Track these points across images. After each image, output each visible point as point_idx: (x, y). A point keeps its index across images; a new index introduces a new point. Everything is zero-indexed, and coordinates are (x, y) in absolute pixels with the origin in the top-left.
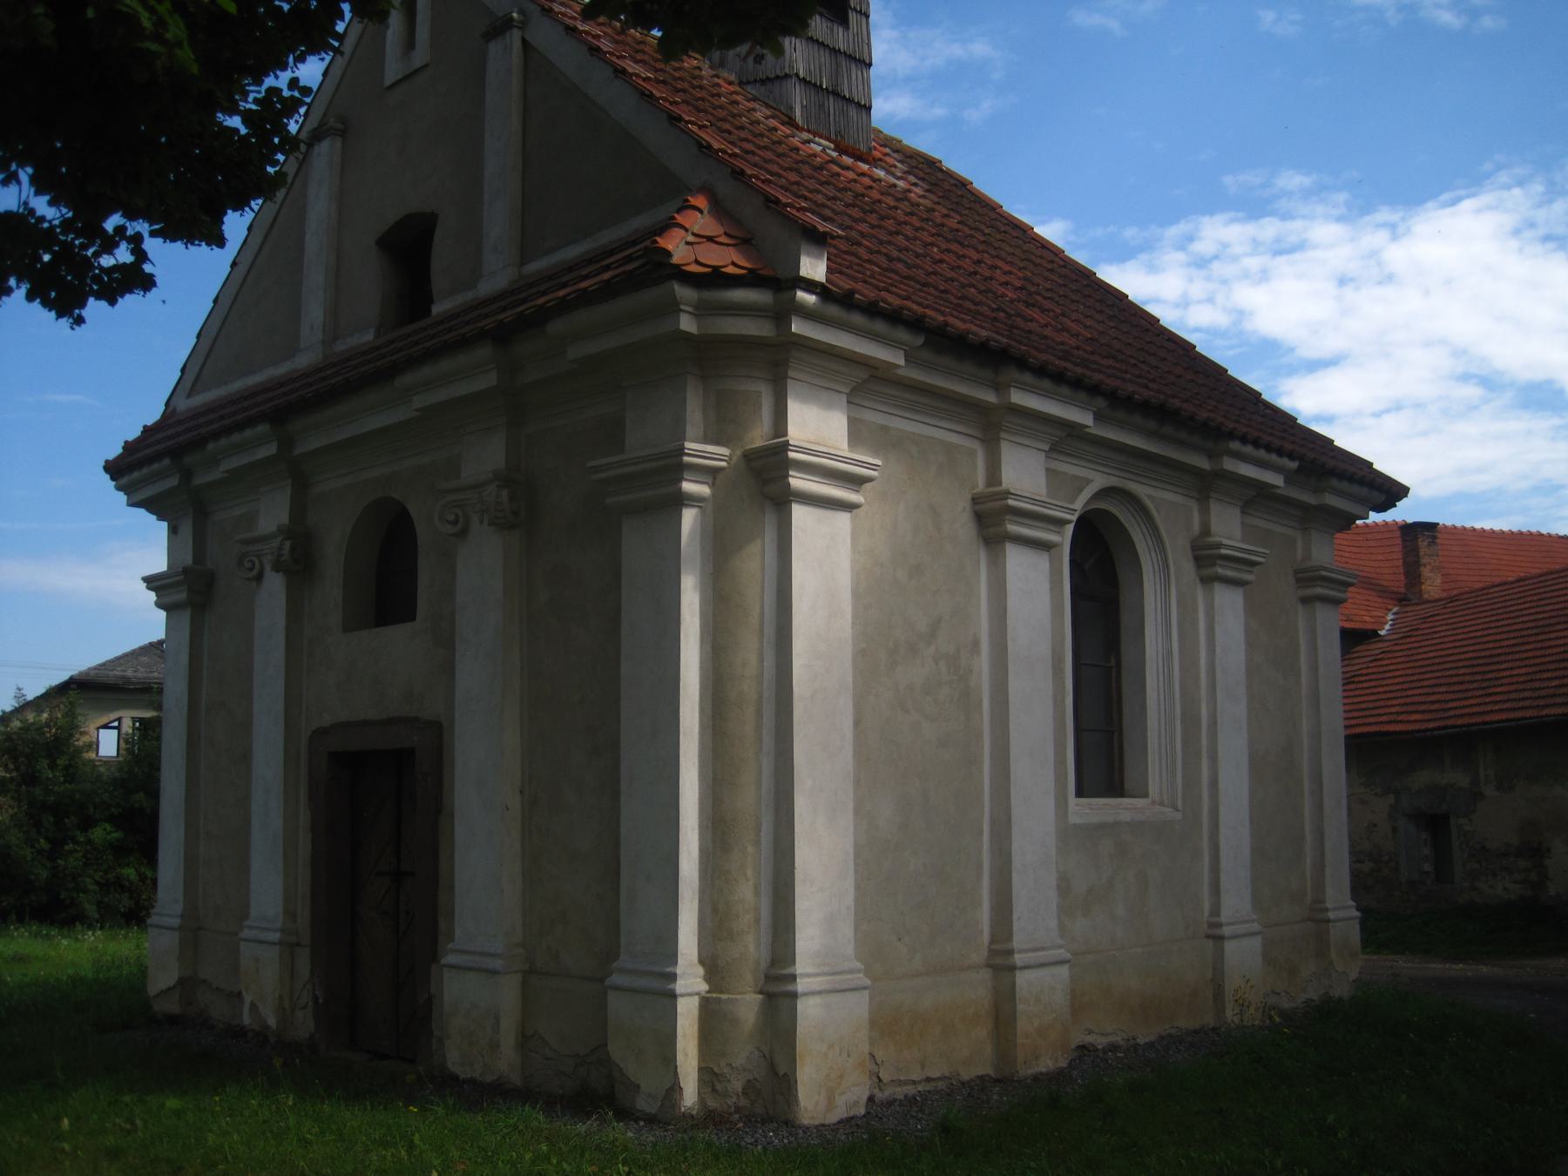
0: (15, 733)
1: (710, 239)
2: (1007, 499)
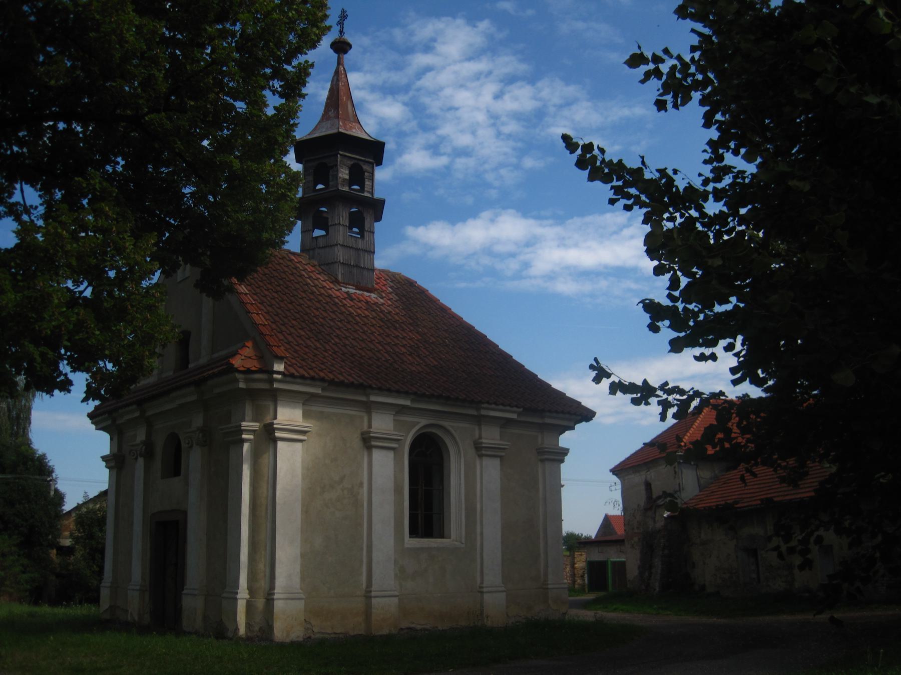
0: (83, 514)
1: (250, 358)
2: (370, 433)
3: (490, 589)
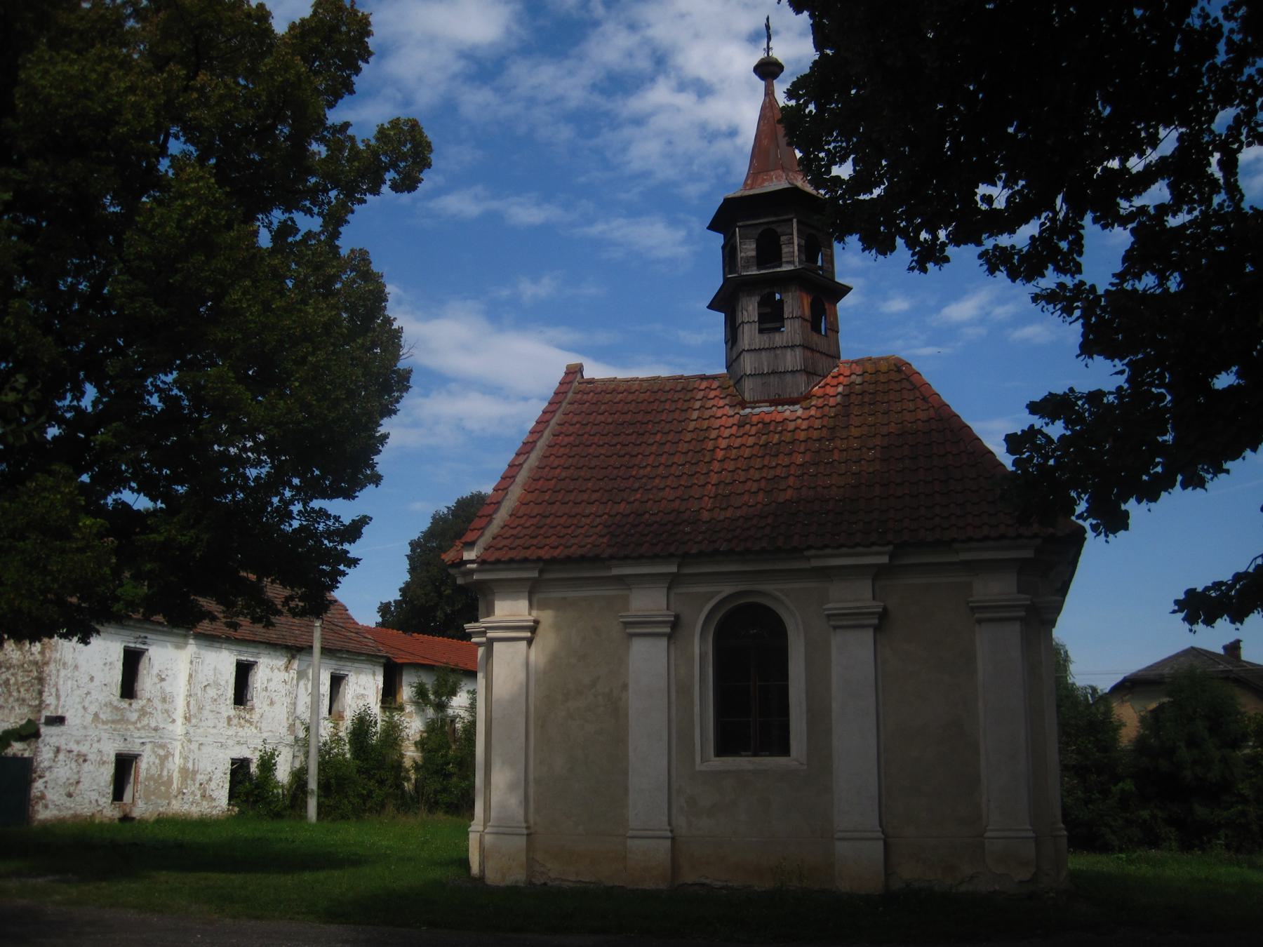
3: (635, 833)
